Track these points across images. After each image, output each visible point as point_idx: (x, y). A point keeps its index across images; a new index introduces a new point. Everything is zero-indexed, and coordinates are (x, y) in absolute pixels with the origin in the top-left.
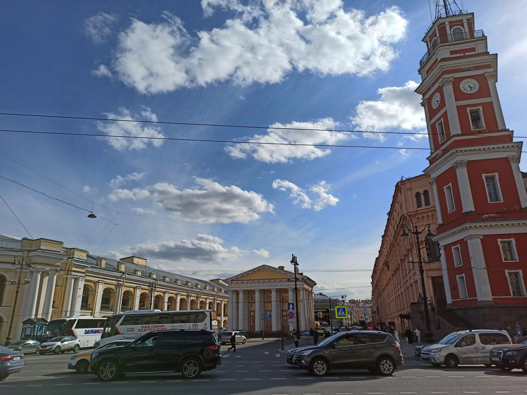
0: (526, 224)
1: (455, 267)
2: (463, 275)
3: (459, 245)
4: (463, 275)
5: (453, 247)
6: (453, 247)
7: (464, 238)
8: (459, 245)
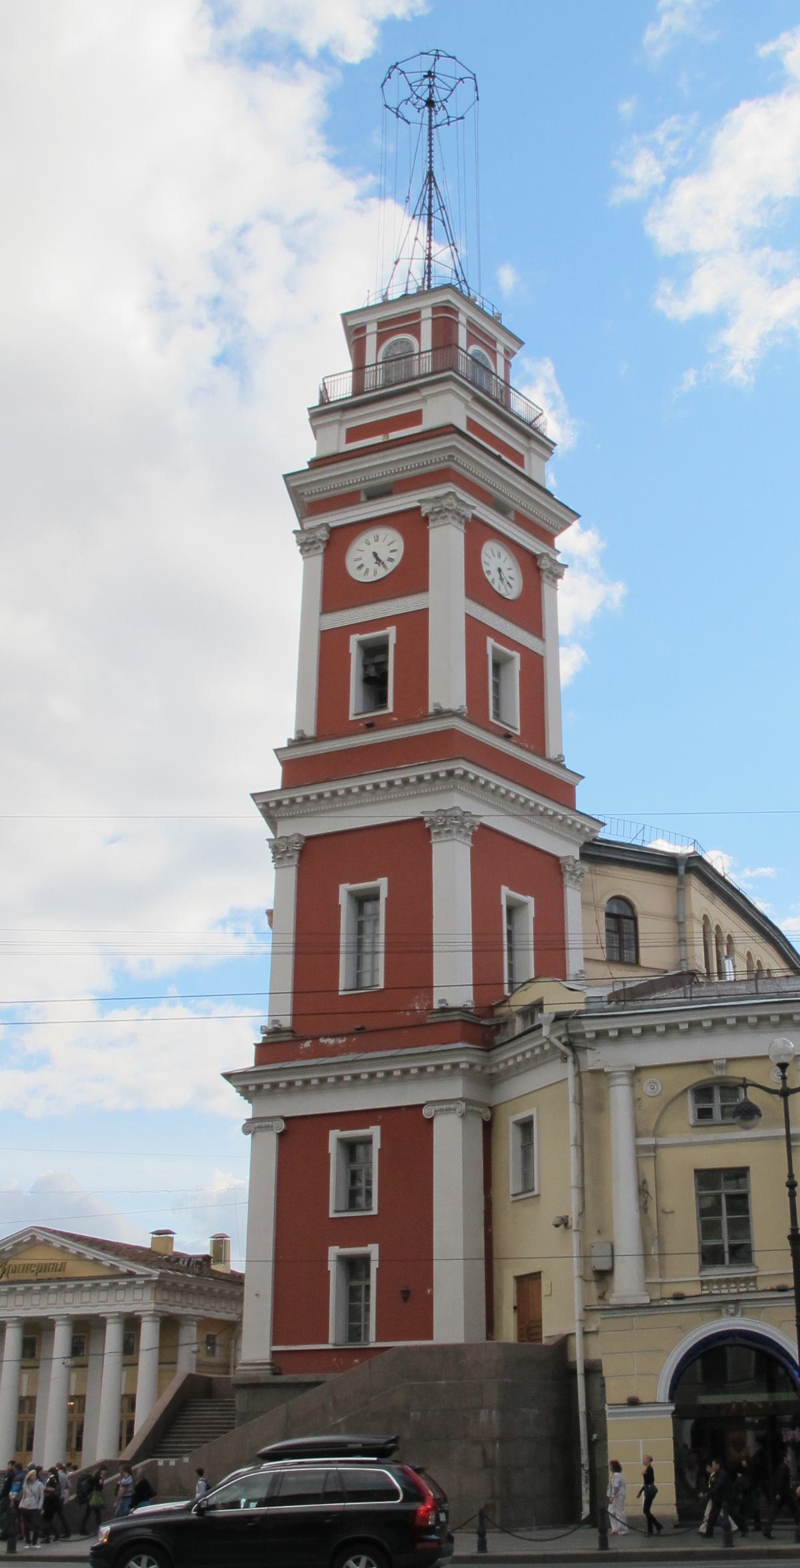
0: (796, 1018)
1: (332, 1215)
2: (373, 1250)
3: (375, 1131)
4: (373, 1250)
5: (334, 1135)
6: (334, 1135)
7: (422, 1106)
8: (375, 1131)
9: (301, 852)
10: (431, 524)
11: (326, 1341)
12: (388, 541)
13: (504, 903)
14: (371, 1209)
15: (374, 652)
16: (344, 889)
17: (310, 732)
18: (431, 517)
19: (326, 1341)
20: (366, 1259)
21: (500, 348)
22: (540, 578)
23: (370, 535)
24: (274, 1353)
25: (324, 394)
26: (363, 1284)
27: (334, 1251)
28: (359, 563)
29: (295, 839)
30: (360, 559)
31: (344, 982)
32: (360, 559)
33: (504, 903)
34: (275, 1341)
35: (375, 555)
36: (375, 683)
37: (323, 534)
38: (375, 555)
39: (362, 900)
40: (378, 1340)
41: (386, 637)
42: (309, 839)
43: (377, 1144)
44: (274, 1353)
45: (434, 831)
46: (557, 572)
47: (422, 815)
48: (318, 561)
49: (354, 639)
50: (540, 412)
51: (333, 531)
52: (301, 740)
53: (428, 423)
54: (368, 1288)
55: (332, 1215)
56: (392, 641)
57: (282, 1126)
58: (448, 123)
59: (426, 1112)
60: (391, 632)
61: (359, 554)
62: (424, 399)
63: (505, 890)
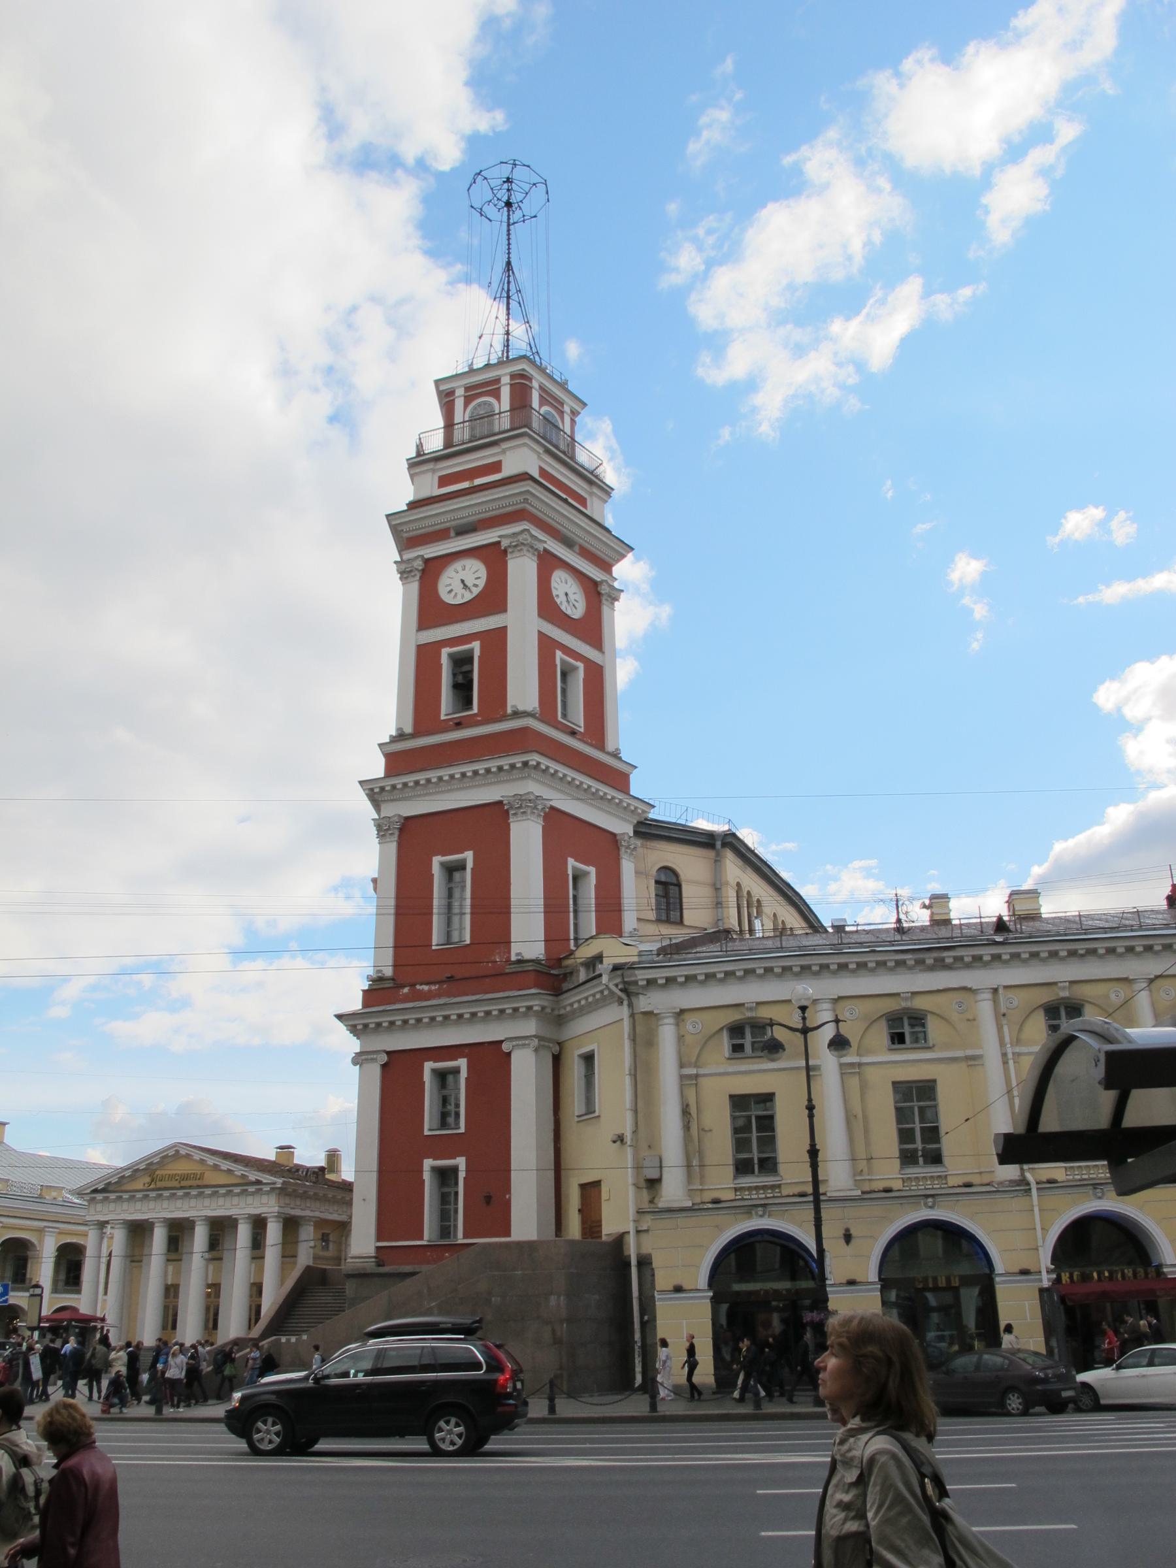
1: (426, 1133)
2: (461, 1162)
3: (462, 1063)
4: (461, 1162)
5: (428, 1066)
6: (428, 1066)
7: (501, 1042)
8: (462, 1063)
9: (401, 830)
10: (509, 556)
11: (421, 1238)
12: (473, 570)
13: (570, 872)
14: (459, 1128)
15: (462, 662)
16: (437, 860)
17: (409, 729)
18: (510, 550)
19: (421, 1238)
20: (456, 1071)
21: (567, 409)
22: (600, 601)
23: (458, 565)
24: (378, 1248)
25: (419, 447)
26: (452, 1190)
27: (428, 1163)
28: (449, 588)
29: (396, 819)
30: (450, 585)
31: (436, 938)
32: (450, 585)
33: (570, 872)
34: (379, 1237)
35: (463, 581)
36: (462, 689)
37: (419, 564)
38: (463, 581)
39: (451, 870)
40: (465, 1237)
41: (472, 651)
42: (407, 818)
43: (464, 1074)
44: (378, 1248)
45: (512, 812)
46: (614, 596)
47: (501, 799)
48: (415, 586)
49: (445, 652)
50: (600, 462)
51: (427, 561)
52: (400, 736)
53: (507, 471)
54: (456, 1193)
55: (426, 1133)
56: (477, 653)
57: (384, 1058)
58: (524, 221)
59: (505, 1047)
60: (476, 646)
61: (448, 581)
62: (504, 452)
63: (571, 862)
